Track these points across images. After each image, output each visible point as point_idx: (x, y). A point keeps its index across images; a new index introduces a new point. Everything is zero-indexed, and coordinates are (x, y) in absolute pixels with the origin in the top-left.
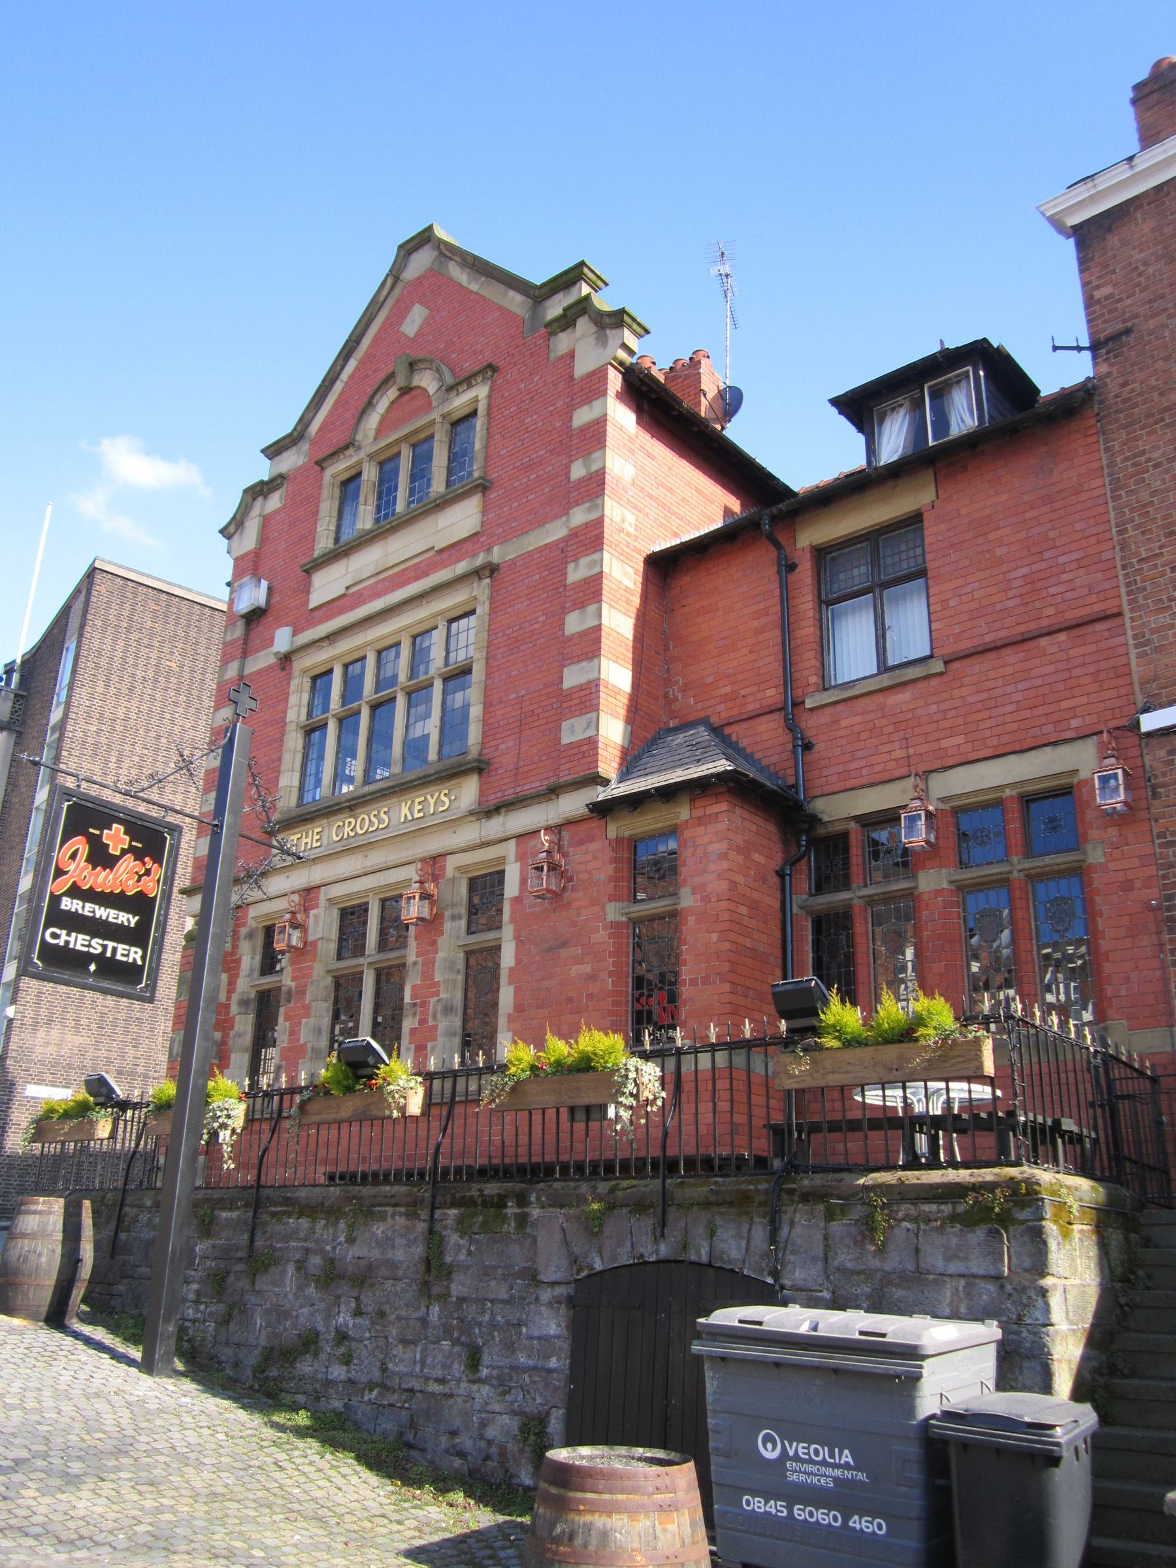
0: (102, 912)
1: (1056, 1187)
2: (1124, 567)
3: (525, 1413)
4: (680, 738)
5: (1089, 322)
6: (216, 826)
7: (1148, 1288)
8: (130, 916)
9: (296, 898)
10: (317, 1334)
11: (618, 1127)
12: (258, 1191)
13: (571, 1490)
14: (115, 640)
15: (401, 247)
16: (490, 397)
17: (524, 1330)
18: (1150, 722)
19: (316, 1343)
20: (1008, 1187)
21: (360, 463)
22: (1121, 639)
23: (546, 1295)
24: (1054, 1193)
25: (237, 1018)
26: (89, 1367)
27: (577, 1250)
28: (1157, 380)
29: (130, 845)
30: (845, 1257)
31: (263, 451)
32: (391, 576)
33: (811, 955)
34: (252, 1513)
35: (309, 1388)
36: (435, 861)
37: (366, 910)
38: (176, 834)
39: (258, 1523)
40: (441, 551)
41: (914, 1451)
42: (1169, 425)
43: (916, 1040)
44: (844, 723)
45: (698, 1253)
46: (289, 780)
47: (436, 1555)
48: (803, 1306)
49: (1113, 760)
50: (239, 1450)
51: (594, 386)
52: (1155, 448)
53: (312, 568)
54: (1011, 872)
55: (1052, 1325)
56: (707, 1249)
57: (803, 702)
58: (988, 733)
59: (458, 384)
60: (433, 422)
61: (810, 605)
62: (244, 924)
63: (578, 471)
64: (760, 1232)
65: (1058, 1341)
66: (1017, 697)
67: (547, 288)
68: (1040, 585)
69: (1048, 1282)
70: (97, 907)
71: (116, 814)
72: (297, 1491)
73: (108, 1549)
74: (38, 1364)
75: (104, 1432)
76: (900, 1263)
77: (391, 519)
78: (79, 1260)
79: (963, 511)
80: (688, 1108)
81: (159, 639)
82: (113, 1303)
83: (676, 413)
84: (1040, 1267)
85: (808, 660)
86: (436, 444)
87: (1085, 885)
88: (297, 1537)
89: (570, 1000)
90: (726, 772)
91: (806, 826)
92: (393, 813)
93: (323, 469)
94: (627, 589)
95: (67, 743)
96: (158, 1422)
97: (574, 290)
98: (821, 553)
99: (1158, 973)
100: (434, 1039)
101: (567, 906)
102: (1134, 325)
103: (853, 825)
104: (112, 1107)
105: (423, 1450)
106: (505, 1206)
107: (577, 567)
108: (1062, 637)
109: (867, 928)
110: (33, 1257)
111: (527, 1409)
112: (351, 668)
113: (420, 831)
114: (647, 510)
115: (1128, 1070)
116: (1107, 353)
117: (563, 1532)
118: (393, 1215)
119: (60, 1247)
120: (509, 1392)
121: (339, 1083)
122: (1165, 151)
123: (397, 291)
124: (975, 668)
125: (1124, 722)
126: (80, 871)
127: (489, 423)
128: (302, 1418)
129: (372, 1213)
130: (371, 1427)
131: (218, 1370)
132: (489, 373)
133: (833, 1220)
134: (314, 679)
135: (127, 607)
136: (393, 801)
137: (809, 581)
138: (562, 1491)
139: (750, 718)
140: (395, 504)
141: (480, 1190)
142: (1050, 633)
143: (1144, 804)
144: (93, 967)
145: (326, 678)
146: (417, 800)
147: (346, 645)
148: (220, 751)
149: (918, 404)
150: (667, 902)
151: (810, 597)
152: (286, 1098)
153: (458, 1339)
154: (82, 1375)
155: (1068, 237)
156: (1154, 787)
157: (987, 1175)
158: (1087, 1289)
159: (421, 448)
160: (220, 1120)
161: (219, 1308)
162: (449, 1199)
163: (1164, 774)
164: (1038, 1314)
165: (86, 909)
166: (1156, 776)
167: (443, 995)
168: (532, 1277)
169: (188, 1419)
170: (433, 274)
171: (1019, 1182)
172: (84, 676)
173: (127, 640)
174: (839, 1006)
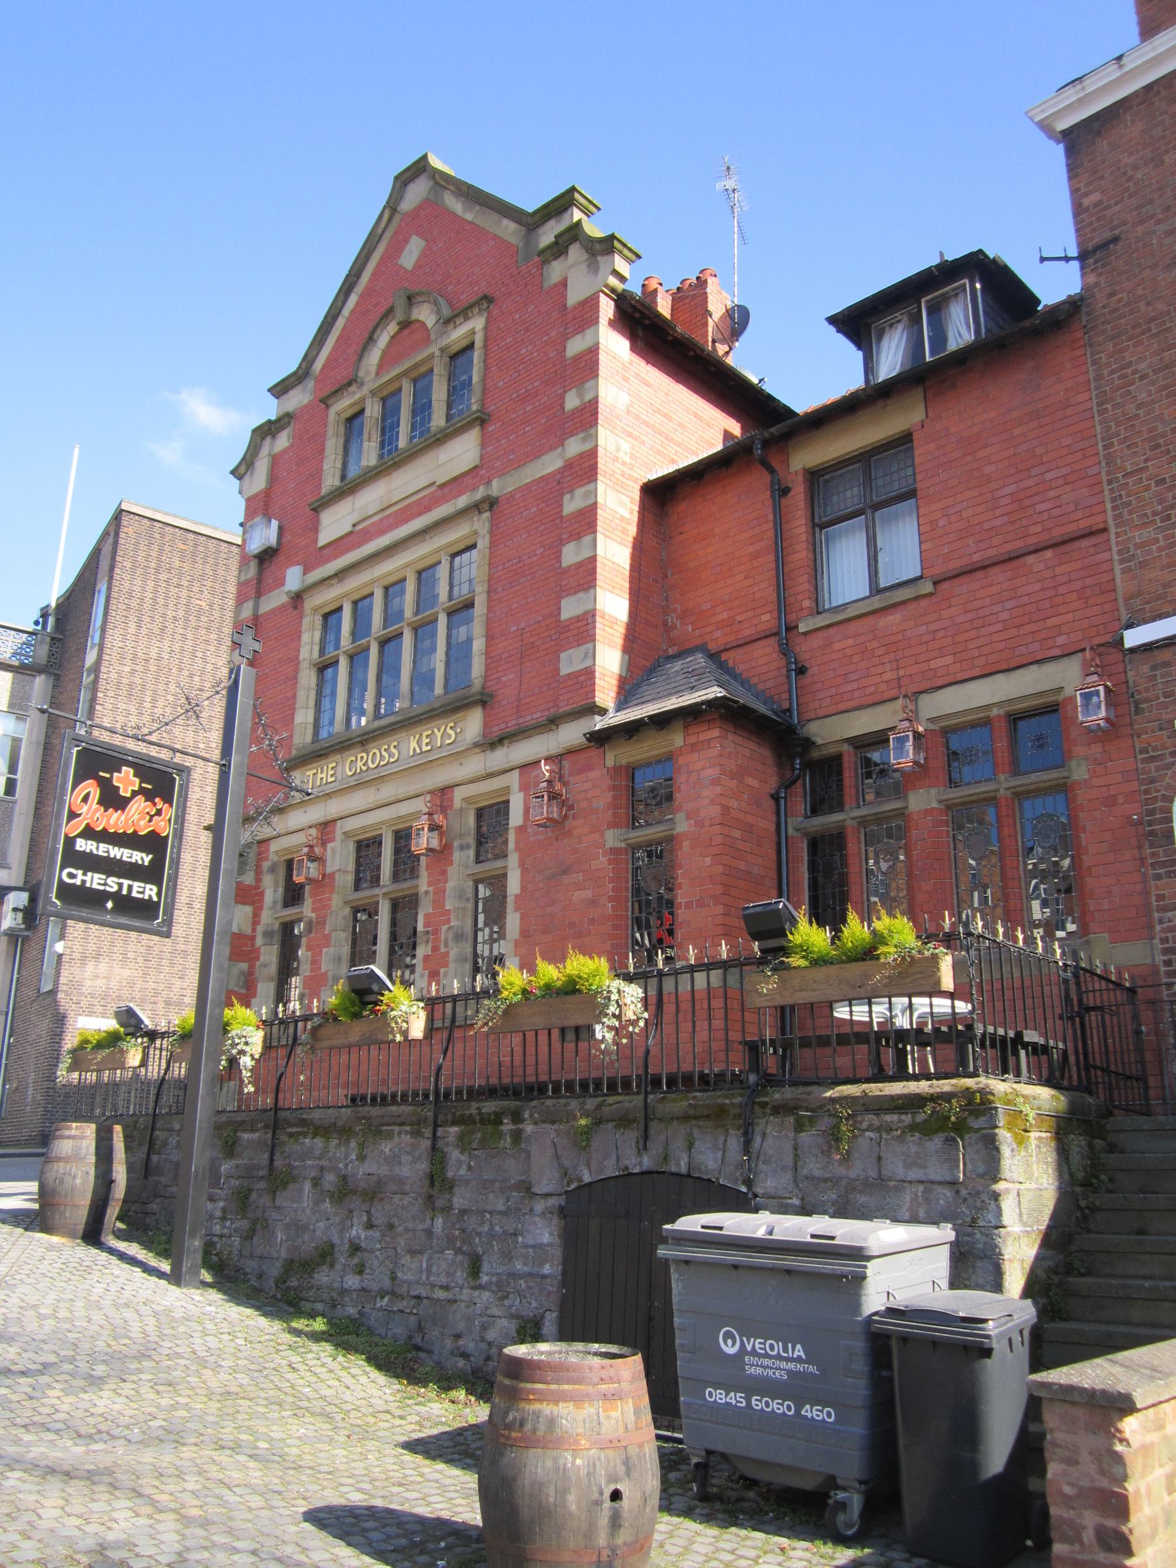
0: (116, 852)
1: (1010, 1097)
2: (1110, 482)
3: (522, 1317)
4: (678, 665)
5: (1077, 231)
6: (224, 765)
7: (1111, 1192)
8: (144, 855)
9: (313, 832)
10: (332, 1246)
11: (603, 1046)
12: (276, 1113)
13: (522, 1381)
14: (144, 581)
15: (397, 178)
16: (486, 328)
17: (520, 1239)
18: (1133, 638)
19: (332, 1254)
20: (964, 1097)
21: (363, 399)
22: (1106, 555)
23: (539, 1206)
24: (1009, 1102)
25: (263, 949)
26: (122, 1280)
27: (567, 1163)
28: (1144, 289)
29: (140, 786)
30: (813, 1167)
31: (270, 390)
32: (395, 512)
33: (806, 876)
34: (262, 1409)
35: (325, 1296)
36: (444, 793)
37: (380, 843)
38: (185, 775)
39: (267, 1419)
40: (442, 486)
41: (859, 1345)
42: (1154, 336)
43: (877, 958)
44: (837, 646)
45: (678, 1164)
46: (304, 716)
47: (432, 1447)
48: (772, 1212)
49: (1095, 678)
50: (256, 1353)
51: (586, 315)
52: (1142, 359)
53: (319, 506)
54: (998, 790)
55: (1003, 1227)
56: (686, 1160)
57: (797, 627)
58: (976, 653)
59: (456, 316)
60: (432, 356)
61: (803, 529)
62: (266, 859)
63: (572, 401)
64: (734, 1143)
65: (1010, 1241)
66: (1005, 616)
67: (538, 215)
68: (1027, 502)
69: (1000, 1186)
70: (111, 847)
71: (125, 757)
72: (308, 1390)
73: (123, 1441)
74: (73, 1278)
75: (130, 1338)
76: (864, 1170)
77: (394, 454)
78: (112, 1181)
79: (952, 430)
80: (668, 1028)
81: (188, 578)
82: (148, 1220)
83: (670, 338)
84: (993, 1172)
85: (802, 584)
86: (435, 377)
87: (1069, 802)
88: (302, 1431)
89: (572, 925)
90: (716, 699)
91: (799, 749)
92: (403, 746)
93: (328, 407)
94: (622, 519)
95: (102, 684)
96: (182, 1329)
97: (566, 216)
98: (814, 476)
99: (1139, 887)
100: (446, 965)
101: (570, 833)
102: (1122, 232)
103: (846, 747)
104: (142, 1036)
105: (429, 1352)
106: (501, 1123)
107: (572, 498)
108: (1048, 554)
109: (860, 848)
110: (68, 1179)
111: (524, 1313)
112: (360, 604)
113: (427, 764)
114: (643, 438)
115: (1103, 982)
116: (1096, 262)
117: (515, 1419)
118: (400, 1133)
119: (93, 1169)
120: (506, 1297)
121: (346, 1009)
122: (1154, 49)
123: (395, 223)
124: (962, 588)
125: (1108, 638)
126: (92, 813)
127: (486, 355)
128: (319, 1325)
129: (380, 1132)
130: (383, 1331)
131: (244, 1282)
132: (485, 305)
133: (802, 1131)
134: (326, 616)
135: (155, 547)
136: (402, 735)
137: (802, 504)
138: (514, 1382)
139: (745, 644)
140: (397, 440)
141: (479, 1109)
142: (1036, 551)
143: (1127, 720)
144: (110, 905)
145: (336, 615)
146: (425, 734)
147: (354, 583)
148: (224, 692)
149: (916, 319)
150: (663, 828)
151: (803, 521)
152: (300, 1024)
153: (460, 1248)
154: (113, 1287)
155: (1058, 142)
156: (1137, 703)
157: (946, 1086)
158: (1044, 1193)
159: (421, 380)
160: (239, 1047)
161: (244, 1224)
162: (450, 1117)
163: (1147, 690)
164: (990, 1217)
165: (102, 849)
166: (1139, 692)
167: (454, 923)
168: (527, 1190)
169: (210, 1326)
170: (430, 205)
171: (974, 1092)
172: (116, 617)
173: (157, 580)
174: (807, 925)
